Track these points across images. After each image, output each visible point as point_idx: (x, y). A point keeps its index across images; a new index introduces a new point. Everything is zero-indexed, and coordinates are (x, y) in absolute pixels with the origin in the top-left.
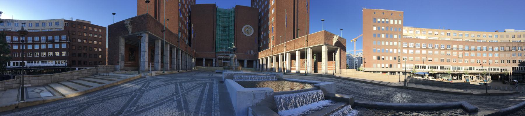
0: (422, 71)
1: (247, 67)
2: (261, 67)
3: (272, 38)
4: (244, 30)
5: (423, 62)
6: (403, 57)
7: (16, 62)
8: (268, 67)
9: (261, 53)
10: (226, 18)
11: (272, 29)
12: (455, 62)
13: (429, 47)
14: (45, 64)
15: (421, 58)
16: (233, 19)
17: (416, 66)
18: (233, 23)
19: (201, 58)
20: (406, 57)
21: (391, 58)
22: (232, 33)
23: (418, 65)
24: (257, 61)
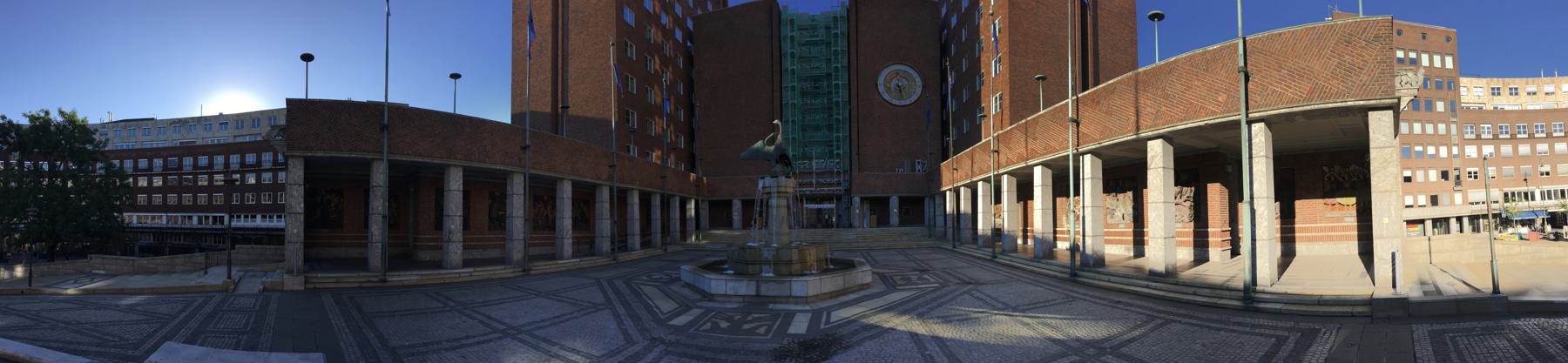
0: (1525, 207)
1: (902, 223)
2: (949, 223)
3: (992, 104)
4: (885, 86)
5: (1525, 180)
6: (1469, 170)
7: (203, 214)
8: (980, 226)
10: (815, 44)
11: (994, 69)
13: (1537, 132)
14: (270, 221)
15: (1517, 170)
16: (841, 45)
17: (1506, 195)
19: (725, 198)
20: (1476, 169)
21: (1433, 175)
22: (842, 96)
23: (1513, 189)
24: (938, 201)
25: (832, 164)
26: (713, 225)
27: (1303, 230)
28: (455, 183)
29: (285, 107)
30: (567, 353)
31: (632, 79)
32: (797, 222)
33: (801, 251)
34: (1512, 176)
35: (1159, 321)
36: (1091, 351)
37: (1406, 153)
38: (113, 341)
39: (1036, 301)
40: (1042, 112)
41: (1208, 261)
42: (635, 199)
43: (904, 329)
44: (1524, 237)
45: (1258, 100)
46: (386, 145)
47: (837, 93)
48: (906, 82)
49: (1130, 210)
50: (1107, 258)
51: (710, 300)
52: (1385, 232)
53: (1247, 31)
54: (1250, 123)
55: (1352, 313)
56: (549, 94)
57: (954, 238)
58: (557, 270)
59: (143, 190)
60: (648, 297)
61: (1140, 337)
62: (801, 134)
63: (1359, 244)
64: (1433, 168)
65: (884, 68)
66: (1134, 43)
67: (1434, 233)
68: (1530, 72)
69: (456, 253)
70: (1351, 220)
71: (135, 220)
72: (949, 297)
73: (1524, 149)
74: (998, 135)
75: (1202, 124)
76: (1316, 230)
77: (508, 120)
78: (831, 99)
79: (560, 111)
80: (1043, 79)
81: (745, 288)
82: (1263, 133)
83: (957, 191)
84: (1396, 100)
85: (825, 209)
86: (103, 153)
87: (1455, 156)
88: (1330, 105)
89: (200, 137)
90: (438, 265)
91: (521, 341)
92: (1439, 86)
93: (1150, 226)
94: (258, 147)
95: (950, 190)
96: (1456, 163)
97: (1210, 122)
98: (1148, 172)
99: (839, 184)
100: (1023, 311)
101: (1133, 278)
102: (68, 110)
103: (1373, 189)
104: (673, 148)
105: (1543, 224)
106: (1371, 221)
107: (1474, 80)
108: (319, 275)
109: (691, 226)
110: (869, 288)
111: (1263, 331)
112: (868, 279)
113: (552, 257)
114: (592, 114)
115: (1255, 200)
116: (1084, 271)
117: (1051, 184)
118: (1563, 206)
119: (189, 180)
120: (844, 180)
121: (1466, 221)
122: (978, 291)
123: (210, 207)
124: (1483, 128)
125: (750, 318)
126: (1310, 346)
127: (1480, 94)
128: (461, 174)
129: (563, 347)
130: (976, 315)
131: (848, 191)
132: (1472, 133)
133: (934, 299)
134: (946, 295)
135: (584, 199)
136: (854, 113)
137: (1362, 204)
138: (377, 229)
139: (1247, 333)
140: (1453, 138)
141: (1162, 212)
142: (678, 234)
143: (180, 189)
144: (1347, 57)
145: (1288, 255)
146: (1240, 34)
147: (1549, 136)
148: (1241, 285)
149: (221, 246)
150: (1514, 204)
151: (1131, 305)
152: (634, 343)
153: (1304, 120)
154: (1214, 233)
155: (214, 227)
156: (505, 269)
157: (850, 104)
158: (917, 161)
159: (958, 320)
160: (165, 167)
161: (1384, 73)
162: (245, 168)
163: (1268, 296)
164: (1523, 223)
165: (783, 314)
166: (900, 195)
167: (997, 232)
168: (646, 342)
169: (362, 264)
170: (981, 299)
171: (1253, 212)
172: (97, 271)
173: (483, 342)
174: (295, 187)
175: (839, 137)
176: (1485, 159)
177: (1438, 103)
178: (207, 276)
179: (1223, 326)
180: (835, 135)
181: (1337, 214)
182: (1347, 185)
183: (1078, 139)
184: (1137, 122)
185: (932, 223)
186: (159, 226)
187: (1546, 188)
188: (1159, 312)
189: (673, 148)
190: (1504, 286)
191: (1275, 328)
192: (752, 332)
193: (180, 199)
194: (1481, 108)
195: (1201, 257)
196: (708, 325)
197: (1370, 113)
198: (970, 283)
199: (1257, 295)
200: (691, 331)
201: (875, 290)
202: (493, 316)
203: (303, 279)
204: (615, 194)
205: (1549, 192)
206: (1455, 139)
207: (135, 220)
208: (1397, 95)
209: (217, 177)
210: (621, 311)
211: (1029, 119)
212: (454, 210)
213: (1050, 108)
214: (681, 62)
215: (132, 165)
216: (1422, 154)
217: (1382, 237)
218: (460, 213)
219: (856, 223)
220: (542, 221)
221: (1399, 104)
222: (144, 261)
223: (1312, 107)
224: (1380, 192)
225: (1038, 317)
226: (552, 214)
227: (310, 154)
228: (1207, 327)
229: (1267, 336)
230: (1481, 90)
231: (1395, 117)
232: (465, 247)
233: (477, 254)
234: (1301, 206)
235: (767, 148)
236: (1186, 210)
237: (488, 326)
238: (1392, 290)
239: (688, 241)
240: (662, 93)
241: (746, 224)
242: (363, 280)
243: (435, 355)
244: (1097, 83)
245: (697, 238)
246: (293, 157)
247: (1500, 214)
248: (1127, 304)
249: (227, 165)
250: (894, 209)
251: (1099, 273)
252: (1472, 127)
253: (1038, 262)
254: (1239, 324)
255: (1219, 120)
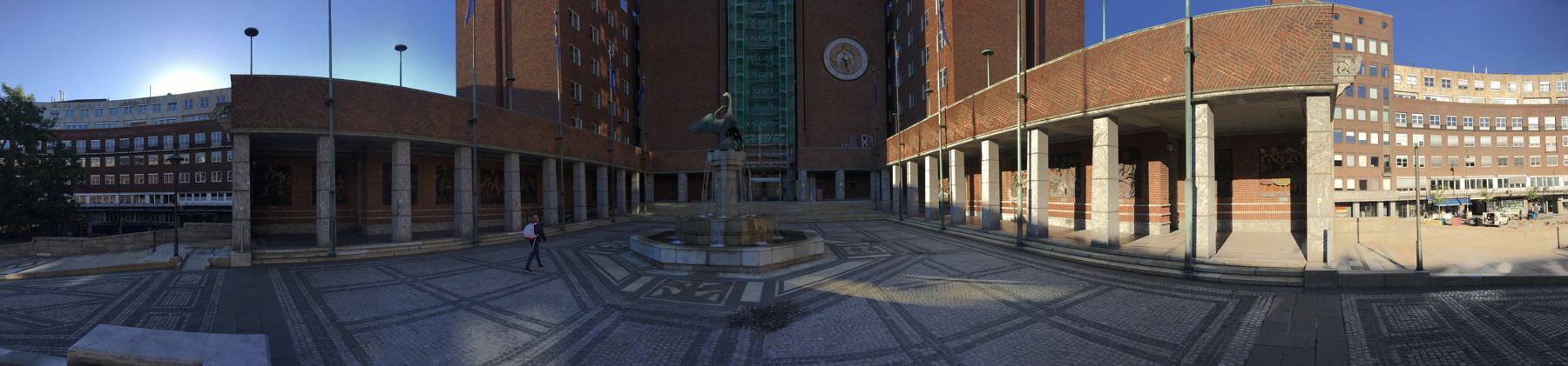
1: (848, 196)
2: (896, 197)
3: (938, 78)
5: (1452, 169)
6: (1398, 157)
7: (139, 194)
8: (927, 199)
9: (894, 142)
10: (762, 17)
11: (938, 42)
12: (1538, 163)
16: (787, 18)
17: (1433, 183)
18: (788, 35)
20: (1406, 157)
21: (1363, 161)
22: (788, 70)
23: (1440, 178)
24: (884, 174)
25: (778, 138)
26: (658, 198)
27: (1239, 208)
28: (402, 158)
29: (229, 85)
30: (525, 322)
31: (576, 50)
32: (741, 196)
33: (751, 223)
34: (1440, 165)
35: (1105, 287)
36: (1041, 312)
37: (1339, 138)
38: (44, 327)
39: (987, 268)
40: (989, 88)
41: (1148, 234)
42: (581, 172)
43: (861, 296)
44: (1447, 222)
45: (1202, 81)
46: (331, 120)
47: (783, 66)
48: (852, 57)
49: (1073, 186)
50: (1050, 229)
51: (659, 268)
52: (1319, 211)
53: (1194, 11)
54: (1194, 103)
55: (1286, 283)
56: (494, 66)
57: (901, 211)
58: (508, 241)
59: (95, 171)
60: (597, 265)
61: (1082, 300)
62: (748, 108)
63: (1292, 223)
64: (1362, 154)
65: (823, 51)
66: (1081, 18)
67: (1361, 216)
68: (1462, 66)
69: (405, 227)
70: (1285, 200)
71: (88, 201)
72: (902, 266)
73: (1453, 140)
74: (945, 111)
75: (1147, 103)
76: (1252, 208)
77: (453, 93)
78: (777, 73)
79: (505, 84)
80: (990, 53)
81: (695, 257)
82: (1206, 114)
83: (903, 167)
84: (1334, 87)
85: (770, 183)
86: (51, 133)
87: (1385, 143)
88: (1272, 90)
89: (150, 118)
90: (387, 238)
91: (475, 312)
92: (1373, 72)
93: (1093, 201)
94: (207, 127)
95: (897, 164)
96: (1387, 150)
97: (1154, 102)
98: (1095, 150)
99: (784, 158)
100: (977, 278)
101: (1075, 248)
102: (13, 86)
103: (1308, 171)
104: (619, 122)
105: (1465, 211)
106: (1306, 201)
107: (1408, 69)
108: (267, 251)
109: (636, 198)
110: (821, 258)
111: (1203, 296)
112: (821, 249)
113: (501, 229)
114: (537, 86)
115: (1197, 178)
116: (1030, 241)
117: (998, 159)
118: (1484, 195)
119: (141, 160)
120: (789, 155)
121: (1393, 206)
122: (931, 260)
123: (161, 186)
124: (1415, 117)
125: (701, 286)
126: (1248, 310)
127: (1414, 83)
128: (409, 149)
129: (519, 317)
130: (932, 282)
131: (794, 165)
132: (1403, 121)
133: (888, 268)
134: (899, 264)
135: (532, 172)
136: (800, 87)
137: (1296, 185)
138: (325, 206)
139: (1188, 298)
140: (1385, 125)
141: (1106, 188)
142: (625, 206)
143: (131, 170)
144: (1289, 42)
145: (1224, 231)
146: (1187, 14)
147: (1476, 129)
148: (1182, 256)
149: (172, 223)
150: (1440, 191)
151: (1073, 272)
152: (587, 310)
153: (1245, 103)
154: (1155, 210)
155: (166, 205)
156: (454, 241)
157: (796, 79)
158: (863, 136)
159: (915, 287)
160: (117, 148)
161: (1323, 60)
162: (194, 148)
163: (1208, 267)
164: (1448, 209)
165: (734, 283)
166: (847, 169)
167: (946, 205)
168: (600, 309)
169: (310, 240)
170: (935, 268)
171: (1195, 190)
172: (42, 254)
173: (435, 315)
174: (240, 164)
175: (785, 112)
176: (1416, 147)
177: (1371, 90)
178: (154, 254)
179: (1166, 292)
180: (781, 110)
181: (1272, 194)
182: (1283, 167)
183: (1026, 115)
184: (1085, 100)
185: (878, 196)
186: (111, 205)
187: (1470, 178)
188: (1104, 279)
189: (619, 122)
190: (1428, 263)
191: (1214, 295)
192: (704, 299)
193: (132, 178)
194: (1413, 98)
195: (1141, 230)
196: (660, 292)
197: (1308, 98)
198: (921, 253)
199: (1196, 266)
200: (642, 297)
201: (826, 260)
202: (444, 288)
203: (250, 255)
204: (562, 167)
205: (1473, 181)
206: (1386, 127)
207: (88, 201)
208: (1335, 81)
209: (166, 157)
210: (573, 279)
211: (976, 94)
212: (402, 184)
213: (998, 84)
214: (626, 33)
215: (85, 146)
216: (1353, 140)
217: (1315, 216)
218: (408, 187)
219: (803, 196)
220: (491, 194)
221: (1336, 90)
222: (93, 241)
223: (1254, 91)
224: (1315, 174)
225: (991, 283)
226: (500, 187)
227: (256, 131)
228: (1150, 292)
229: (1207, 301)
230: (1414, 79)
231: (1331, 103)
232: (413, 221)
233: (425, 227)
234: (1238, 185)
235: (716, 120)
236: (1127, 188)
237: (440, 298)
238: (1324, 264)
239: (633, 213)
240: (608, 64)
241: (693, 196)
242: (313, 255)
243: (385, 330)
244: (1042, 61)
245: (642, 210)
246: (238, 134)
247: (1427, 201)
248: (1069, 271)
249: (176, 144)
250: (840, 182)
251: (1044, 243)
252: (1403, 116)
253: (986, 233)
254: (1180, 291)
255: (1164, 101)
